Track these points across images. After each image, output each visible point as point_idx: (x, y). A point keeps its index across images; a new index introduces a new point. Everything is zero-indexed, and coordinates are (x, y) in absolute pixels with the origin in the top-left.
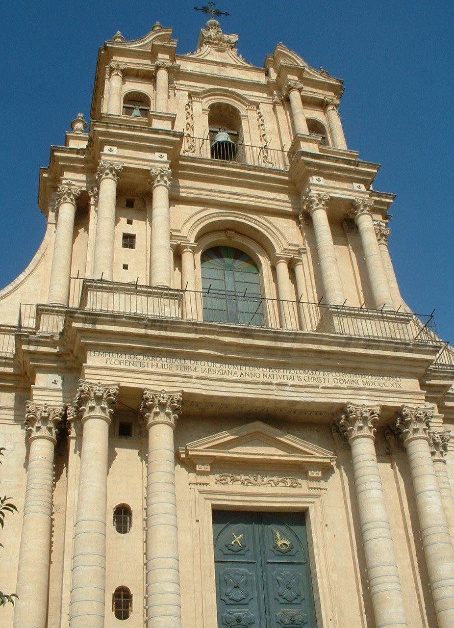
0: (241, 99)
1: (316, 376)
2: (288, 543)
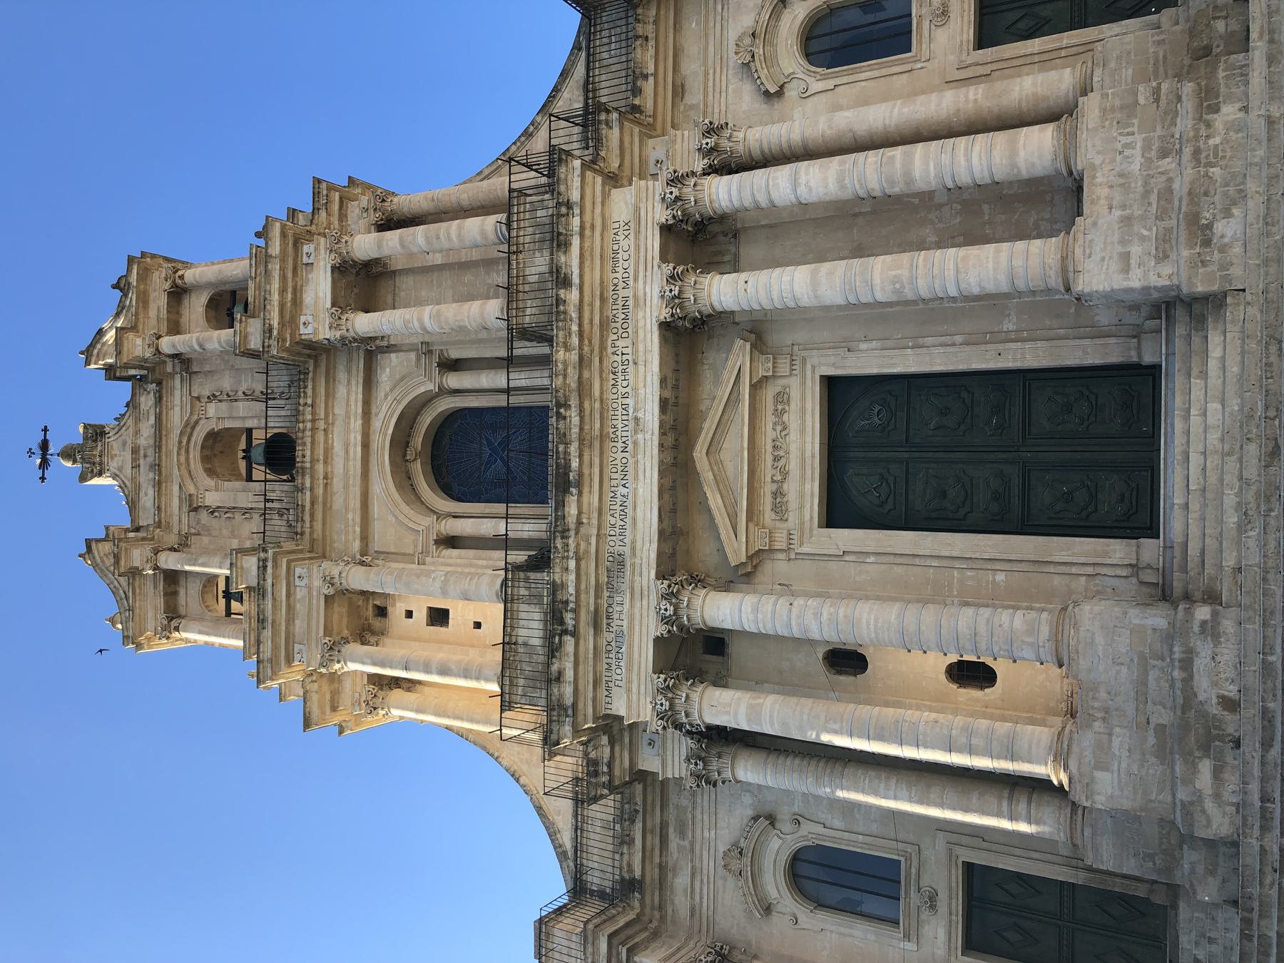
0: (189, 427)
1: (620, 368)
2: (877, 408)
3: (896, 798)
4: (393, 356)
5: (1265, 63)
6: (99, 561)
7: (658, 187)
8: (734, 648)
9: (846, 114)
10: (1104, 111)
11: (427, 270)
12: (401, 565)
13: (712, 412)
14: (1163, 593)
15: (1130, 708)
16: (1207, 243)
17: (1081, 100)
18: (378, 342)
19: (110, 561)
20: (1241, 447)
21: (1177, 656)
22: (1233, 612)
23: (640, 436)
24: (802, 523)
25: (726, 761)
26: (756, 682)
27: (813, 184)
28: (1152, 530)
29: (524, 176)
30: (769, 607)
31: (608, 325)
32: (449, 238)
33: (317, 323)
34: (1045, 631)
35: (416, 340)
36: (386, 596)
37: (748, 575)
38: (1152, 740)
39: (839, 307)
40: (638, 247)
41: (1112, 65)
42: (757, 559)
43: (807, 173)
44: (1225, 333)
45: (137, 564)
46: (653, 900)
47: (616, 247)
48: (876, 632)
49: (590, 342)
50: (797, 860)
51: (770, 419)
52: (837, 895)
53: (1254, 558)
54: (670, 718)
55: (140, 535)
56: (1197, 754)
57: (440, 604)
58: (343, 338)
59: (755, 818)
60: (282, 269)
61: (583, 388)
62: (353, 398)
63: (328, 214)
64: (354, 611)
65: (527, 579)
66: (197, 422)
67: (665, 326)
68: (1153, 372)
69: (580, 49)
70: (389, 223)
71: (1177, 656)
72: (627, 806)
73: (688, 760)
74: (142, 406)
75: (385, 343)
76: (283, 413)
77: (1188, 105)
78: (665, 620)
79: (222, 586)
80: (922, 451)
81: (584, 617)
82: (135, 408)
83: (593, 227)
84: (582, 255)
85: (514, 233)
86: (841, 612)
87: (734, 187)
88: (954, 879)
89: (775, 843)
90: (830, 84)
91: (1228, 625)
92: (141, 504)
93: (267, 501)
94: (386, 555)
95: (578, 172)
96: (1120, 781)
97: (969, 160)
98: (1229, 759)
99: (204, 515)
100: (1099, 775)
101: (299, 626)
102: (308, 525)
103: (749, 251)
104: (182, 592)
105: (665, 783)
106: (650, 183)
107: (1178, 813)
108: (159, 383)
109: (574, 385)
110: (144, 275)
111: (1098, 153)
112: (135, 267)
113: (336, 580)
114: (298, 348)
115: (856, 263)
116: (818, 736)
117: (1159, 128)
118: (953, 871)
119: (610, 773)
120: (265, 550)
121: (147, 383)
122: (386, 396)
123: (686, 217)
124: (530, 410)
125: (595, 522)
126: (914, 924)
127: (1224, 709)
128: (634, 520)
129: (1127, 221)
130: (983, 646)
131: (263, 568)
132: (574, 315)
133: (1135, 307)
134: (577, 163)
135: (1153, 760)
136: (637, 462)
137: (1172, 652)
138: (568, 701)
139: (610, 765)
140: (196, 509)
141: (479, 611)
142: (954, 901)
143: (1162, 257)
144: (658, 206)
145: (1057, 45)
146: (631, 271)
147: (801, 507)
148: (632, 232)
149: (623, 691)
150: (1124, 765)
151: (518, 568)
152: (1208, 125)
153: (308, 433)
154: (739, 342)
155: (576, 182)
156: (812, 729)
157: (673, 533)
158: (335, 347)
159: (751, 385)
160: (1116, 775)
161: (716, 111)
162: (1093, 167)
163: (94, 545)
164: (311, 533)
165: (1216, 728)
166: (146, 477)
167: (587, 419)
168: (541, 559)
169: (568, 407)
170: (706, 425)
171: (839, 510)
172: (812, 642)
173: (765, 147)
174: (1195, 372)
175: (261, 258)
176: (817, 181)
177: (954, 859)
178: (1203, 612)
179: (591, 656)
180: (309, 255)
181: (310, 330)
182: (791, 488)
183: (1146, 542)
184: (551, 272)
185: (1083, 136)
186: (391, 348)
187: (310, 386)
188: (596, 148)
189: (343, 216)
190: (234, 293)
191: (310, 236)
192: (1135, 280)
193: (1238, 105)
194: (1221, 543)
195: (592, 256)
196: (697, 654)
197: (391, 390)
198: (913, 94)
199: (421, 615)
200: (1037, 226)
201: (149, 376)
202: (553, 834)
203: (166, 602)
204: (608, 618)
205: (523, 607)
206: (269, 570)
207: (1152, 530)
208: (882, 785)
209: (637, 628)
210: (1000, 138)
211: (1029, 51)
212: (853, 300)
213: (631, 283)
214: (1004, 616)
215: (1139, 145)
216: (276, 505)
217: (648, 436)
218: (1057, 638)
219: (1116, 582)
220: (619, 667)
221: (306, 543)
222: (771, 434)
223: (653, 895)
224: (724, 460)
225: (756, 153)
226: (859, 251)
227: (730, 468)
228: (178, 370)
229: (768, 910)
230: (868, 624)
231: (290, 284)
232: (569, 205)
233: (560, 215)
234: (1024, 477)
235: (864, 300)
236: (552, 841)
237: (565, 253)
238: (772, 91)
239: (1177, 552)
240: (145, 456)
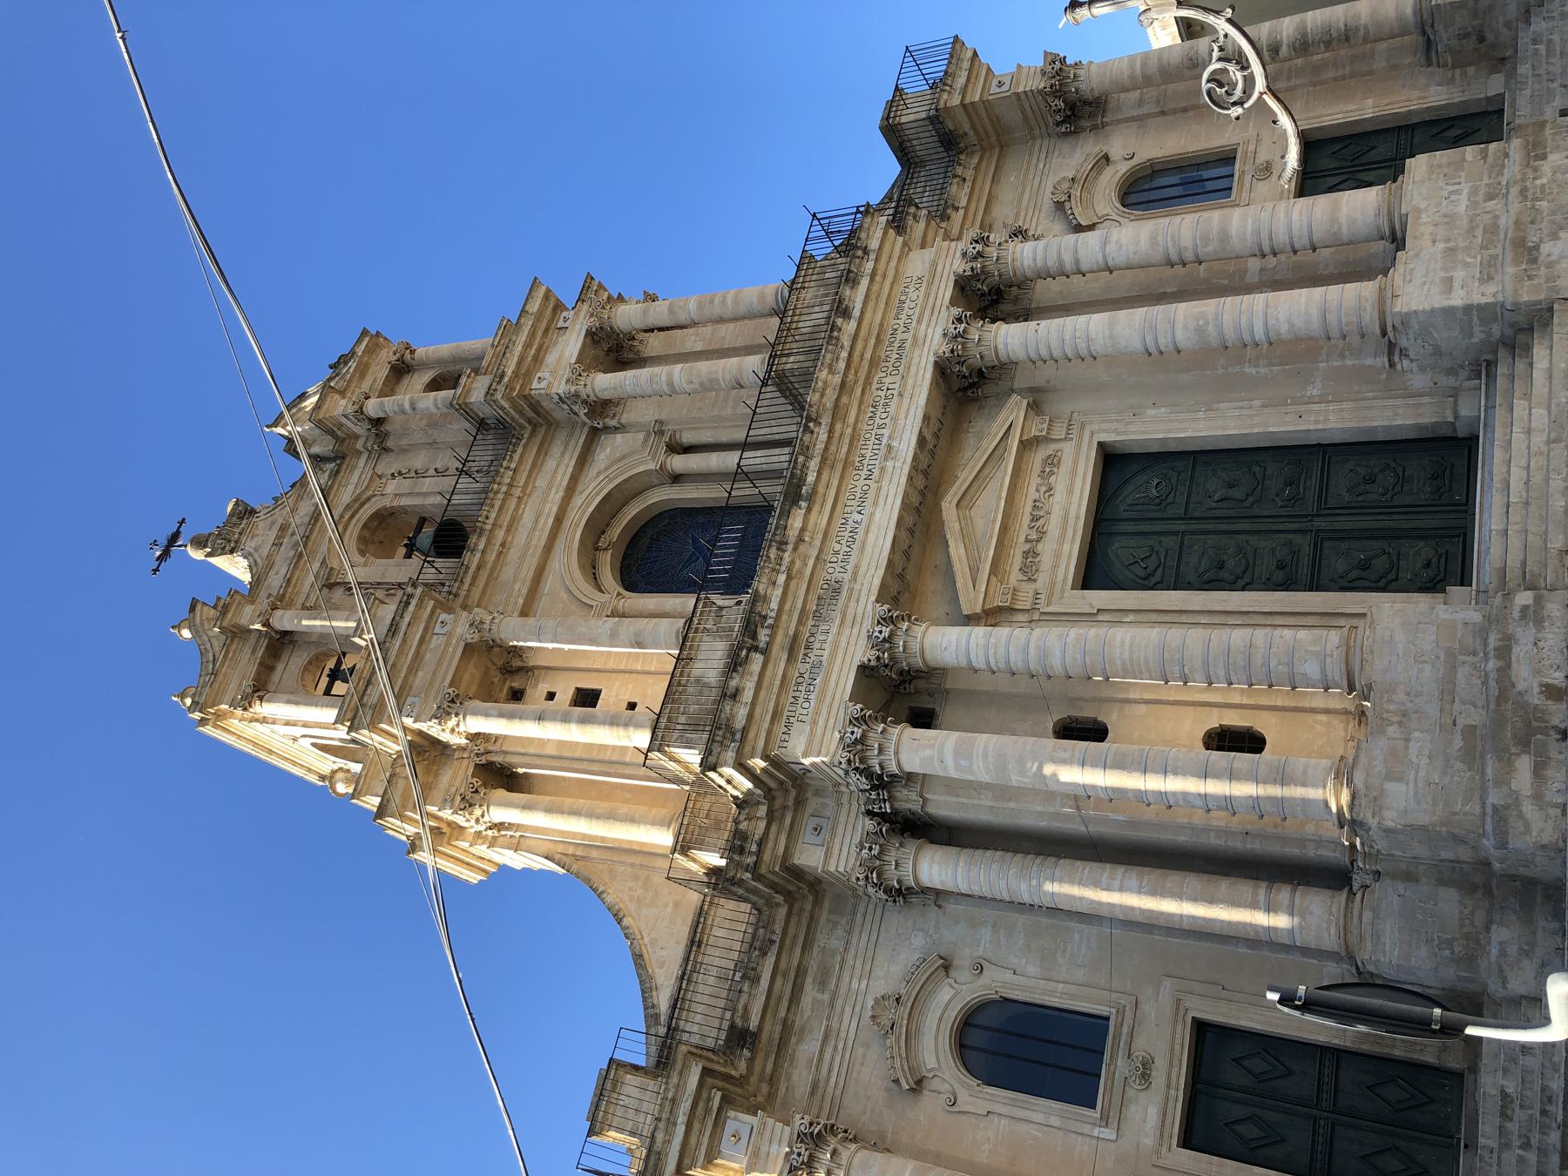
0: (359, 502)
3: (1121, 889)
4: (619, 436)
15: (1432, 710)
21: (1492, 646)
23: (889, 464)
24: (1053, 583)
27: (1124, 242)
31: (878, 365)
32: (724, 302)
38: (1458, 742)
44: (1551, 347)
46: (764, 1068)
48: (1131, 651)
51: (1035, 480)
56: (1514, 750)
57: (589, 683)
61: (838, 411)
62: (561, 470)
66: (369, 499)
69: (891, 199)
71: (1492, 646)
72: (761, 931)
83: (884, 276)
84: (867, 296)
88: (1178, 1041)
91: (1553, 608)
96: (1416, 793)
98: (1553, 754)
100: (1391, 786)
101: (421, 677)
102: (466, 587)
104: (280, 667)
107: (1489, 820)
109: (829, 405)
113: (486, 626)
118: (1179, 1029)
119: (759, 853)
120: (414, 586)
122: (598, 474)
125: (818, 543)
126: (1117, 1100)
127: (1548, 698)
128: (864, 544)
129: (1450, 252)
135: (1459, 765)
136: (879, 488)
137: (1485, 645)
138: (739, 722)
139: (760, 844)
142: (1175, 1070)
143: (1487, 278)
147: (1055, 567)
150: (1422, 774)
152: (1536, 170)
153: (500, 496)
155: (879, 233)
159: (1021, 442)
160: (1411, 785)
162: (1418, 211)
163: (199, 607)
164: (467, 597)
165: (1541, 719)
166: (286, 552)
167: (835, 441)
177: (1181, 1013)
179: (778, 682)
181: (544, 384)
182: (1046, 549)
187: (519, 451)
192: (1458, 299)
196: (903, 692)
197: (606, 469)
202: (647, 989)
203: (258, 673)
206: (411, 608)
208: (1106, 875)
209: (840, 656)
215: (1466, 191)
220: (807, 700)
222: (1032, 494)
223: (766, 1060)
227: (979, 524)
229: (918, 1085)
232: (866, 251)
236: (645, 999)
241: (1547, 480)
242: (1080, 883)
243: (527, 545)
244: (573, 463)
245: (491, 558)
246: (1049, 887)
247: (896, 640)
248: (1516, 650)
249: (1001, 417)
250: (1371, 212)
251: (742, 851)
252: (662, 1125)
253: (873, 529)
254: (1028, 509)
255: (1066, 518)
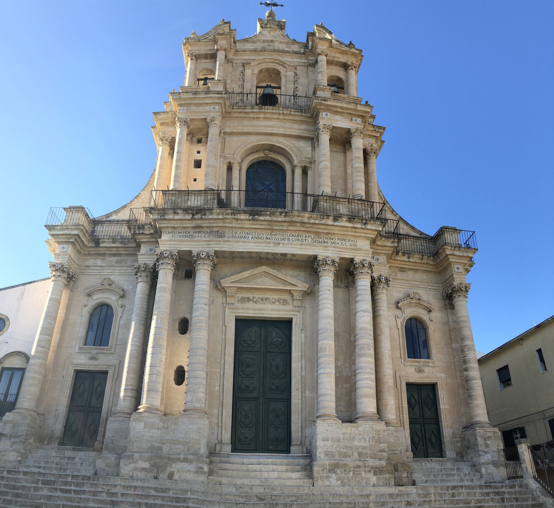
0: (283, 64)
1: (300, 238)
2: (280, 340)
3: (132, 345)
4: (310, 148)
5: (390, 493)
6: (221, 27)
7: (369, 259)
8: (188, 282)
9: (388, 332)
10: (379, 431)
11: (345, 165)
12: (219, 148)
13: (280, 274)
14: (212, 453)
16: (330, 471)
17: (384, 422)
18: (316, 143)
19: (221, 31)
20: (263, 486)
22: (206, 481)
23: (272, 245)
24: (237, 309)
25: (145, 279)
26: (175, 291)
28: (234, 449)
29: (378, 208)
30: (204, 296)
32: (357, 176)
33: (326, 120)
34: (198, 405)
35: (316, 159)
36: (206, 142)
37: (217, 287)
38: (156, 445)
39: (317, 327)
40: (346, 249)
41: (395, 434)
42: (223, 290)
43: (368, 316)
45: (219, 42)
47: (347, 240)
49: (311, 227)
50: (108, 306)
52: (95, 321)
53: (225, 490)
54: (161, 257)
55: (232, 43)
56: (152, 462)
58: (319, 129)
59: (123, 290)
60: (351, 109)
62: (293, 131)
63: (372, 131)
64: (200, 130)
65: (214, 199)
66: (285, 67)
67: (315, 257)
68: (288, 451)
70: (366, 153)
73: (145, 264)
74: (293, 46)
75: (316, 146)
76: (287, 102)
77: (377, 463)
78: (198, 255)
79: (209, 77)
80: (263, 350)
81: (199, 222)
82: (293, 43)
83: (356, 232)
85: (356, 201)
86: (203, 324)
87: (366, 288)
89: (114, 298)
90: (399, 327)
91: (202, 478)
92: (247, 44)
93: (247, 94)
94: (224, 142)
95: (377, 229)
96: (141, 432)
97: (366, 379)
98: (150, 474)
99: (241, 69)
100: (142, 424)
101: (193, 108)
102: (237, 111)
103: (341, 292)
104: (207, 61)
105: (136, 255)
106: (370, 256)
108: (304, 53)
109: (294, 219)
110: (354, 54)
111: (364, 429)
112: (358, 52)
113: (213, 122)
114: (316, 111)
115: (332, 334)
116: (156, 314)
117: (370, 452)
118: (105, 367)
119: (139, 234)
120: (226, 93)
121: (305, 48)
123: (355, 268)
124: (285, 201)
125: (238, 226)
126: (85, 351)
128: (239, 242)
129: (339, 441)
130: (191, 380)
131: (218, 93)
132: (322, 222)
133: (311, 444)
134: (380, 229)
135: (149, 445)
137: (190, 454)
138: (167, 217)
140: (243, 66)
141: (201, 180)
144: (362, 258)
145: (404, 413)
146: (338, 246)
147: (243, 309)
148: (352, 247)
149: (171, 238)
151: (219, 195)
152: (369, 471)
153: (278, 112)
154: (307, 286)
156: (158, 312)
157: (233, 257)
158: (316, 125)
161: (394, 283)
164: (234, 112)
166: (259, 46)
167: (280, 224)
168: (222, 204)
169: (285, 216)
170: (275, 271)
171: (242, 324)
172: (191, 312)
173: (379, 301)
174: (288, 467)
175: (357, 101)
176: (364, 320)
178: (206, 468)
179: (184, 225)
180: (356, 120)
181: (324, 116)
182: (250, 305)
183: (230, 447)
184: (340, 214)
185: (371, 423)
186: (314, 148)
188: (385, 237)
189: (370, 136)
190: (343, 88)
191: (364, 122)
193: (376, 483)
194: (230, 477)
195: (345, 231)
197: (295, 146)
198: (393, 359)
199: (198, 157)
200: (340, 405)
201: (308, 50)
202: (116, 212)
203: (201, 55)
204: (199, 232)
205: (203, 198)
207: (234, 449)
208: (136, 339)
209: (195, 243)
210: (374, 391)
211: (403, 403)
212: (320, 332)
213: (333, 245)
214: (203, 389)
216: (245, 98)
217: (272, 248)
218: (195, 410)
219: (216, 434)
220: (180, 237)
221: (228, 110)
222: (271, 297)
223: (94, 251)
224: (263, 278)
225: (377, 297)
226: (337, 335)
227: (258, 280)
228: (310, 61)
229: (89, 295)
230: (199, 335)
231: (345, 111)
232: (365, 224)
233: (362, 220)
234: (255, 398)
235: (319, 336)
237: (347, 220)
238: (399, 305)
239: (227, 459)
240: (269, 45)
241: (53, 475)
242: (134, 332)
243: (258, 126)
244: (296, 134)
245: (251, 115)
246: (133, 323)
247: (202, 260)
248: (187, 464)
249: (299, 282)
250: (365, 410)
251: (139, 228)
252: (61, 227)
253: (245, 244)
254: (266, 296)
255: (262, 310)
